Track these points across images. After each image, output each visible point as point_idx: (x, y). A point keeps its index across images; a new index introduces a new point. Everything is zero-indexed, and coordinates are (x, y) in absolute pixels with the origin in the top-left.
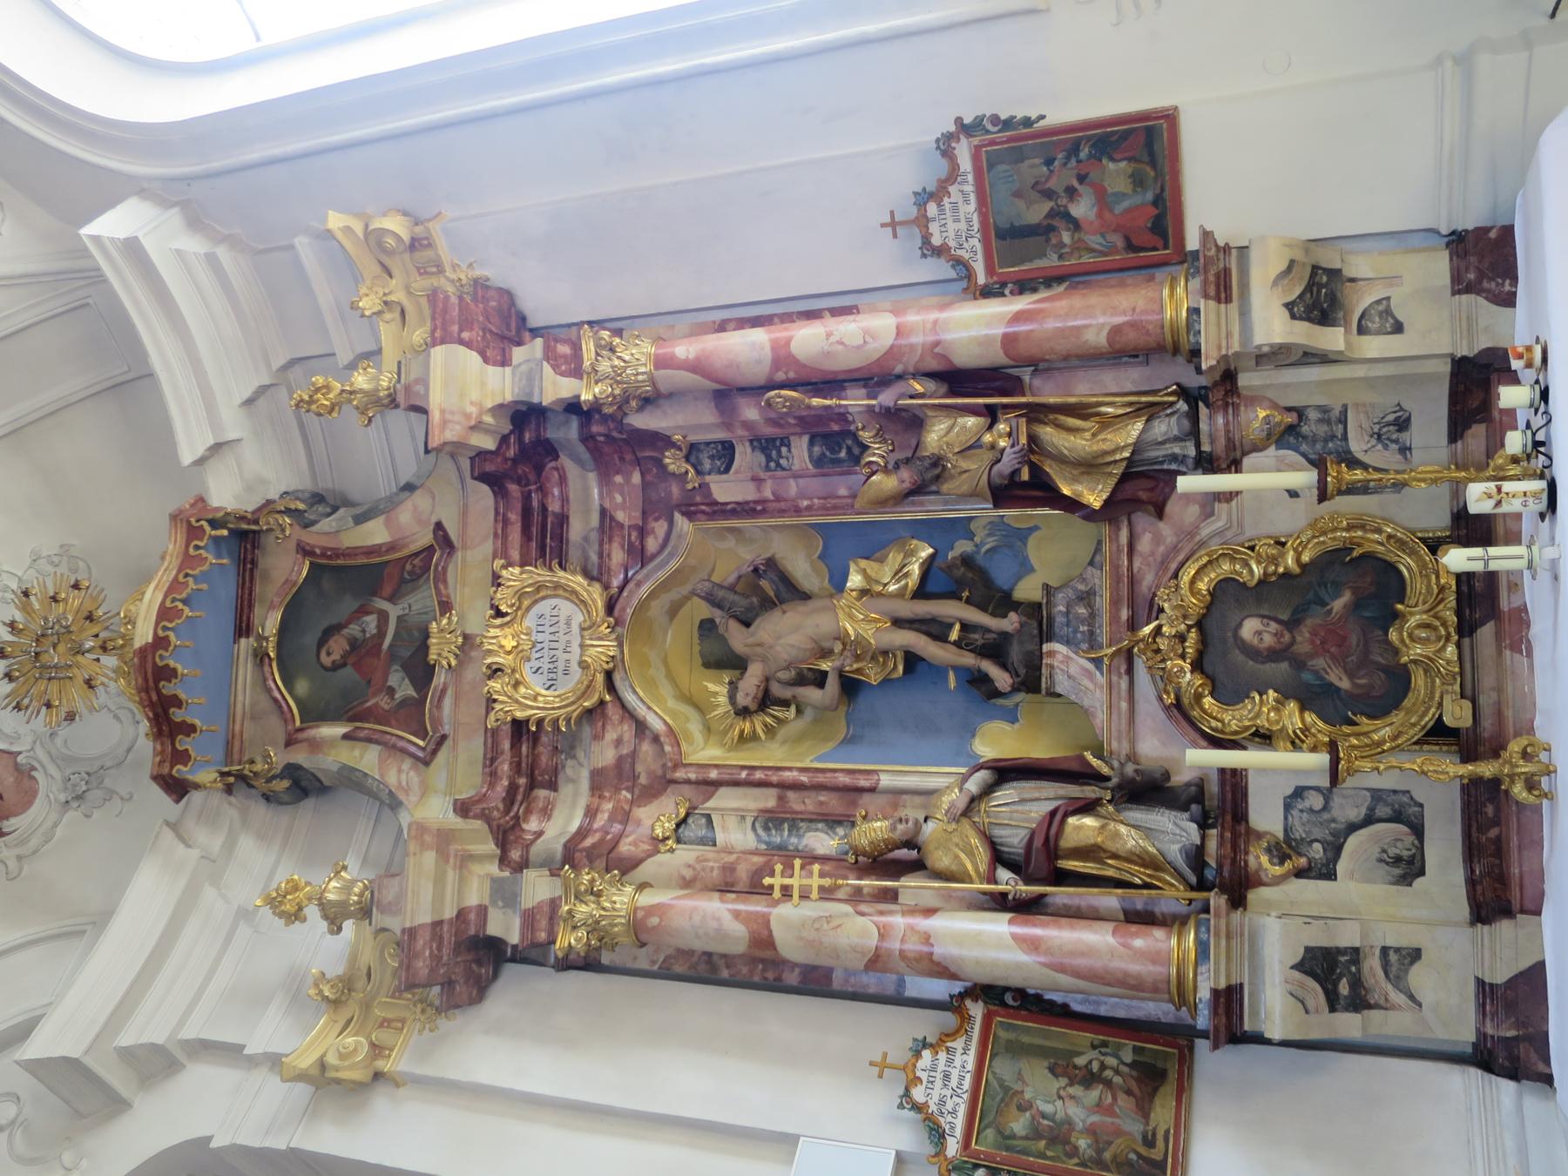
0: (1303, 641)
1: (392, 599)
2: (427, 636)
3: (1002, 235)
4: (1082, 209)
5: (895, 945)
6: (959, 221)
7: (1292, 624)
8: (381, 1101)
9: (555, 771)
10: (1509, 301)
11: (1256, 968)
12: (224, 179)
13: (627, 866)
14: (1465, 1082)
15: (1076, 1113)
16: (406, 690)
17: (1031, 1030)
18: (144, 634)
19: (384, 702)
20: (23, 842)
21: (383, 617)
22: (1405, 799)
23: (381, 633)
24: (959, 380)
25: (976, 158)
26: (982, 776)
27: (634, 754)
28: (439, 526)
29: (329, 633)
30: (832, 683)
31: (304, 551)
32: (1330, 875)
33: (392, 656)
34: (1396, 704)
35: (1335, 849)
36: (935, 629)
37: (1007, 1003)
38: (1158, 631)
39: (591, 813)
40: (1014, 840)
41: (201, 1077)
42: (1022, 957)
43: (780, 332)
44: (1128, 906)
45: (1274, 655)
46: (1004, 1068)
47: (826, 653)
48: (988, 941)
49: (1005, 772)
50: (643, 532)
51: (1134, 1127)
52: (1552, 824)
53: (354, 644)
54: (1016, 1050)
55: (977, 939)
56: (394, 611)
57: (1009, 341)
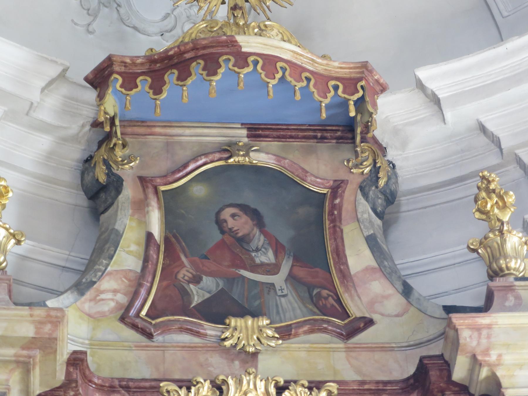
1: (291, 277)
2: (255, 315)
16: (198, 295)
18: (249, 43)
19: (185, 273)
23: (255, 268)
28: (369, 322)
29: (256, 216)
31: (337, 188)
33: (233, 280)
53: (243, 241)
56: (278, 280)
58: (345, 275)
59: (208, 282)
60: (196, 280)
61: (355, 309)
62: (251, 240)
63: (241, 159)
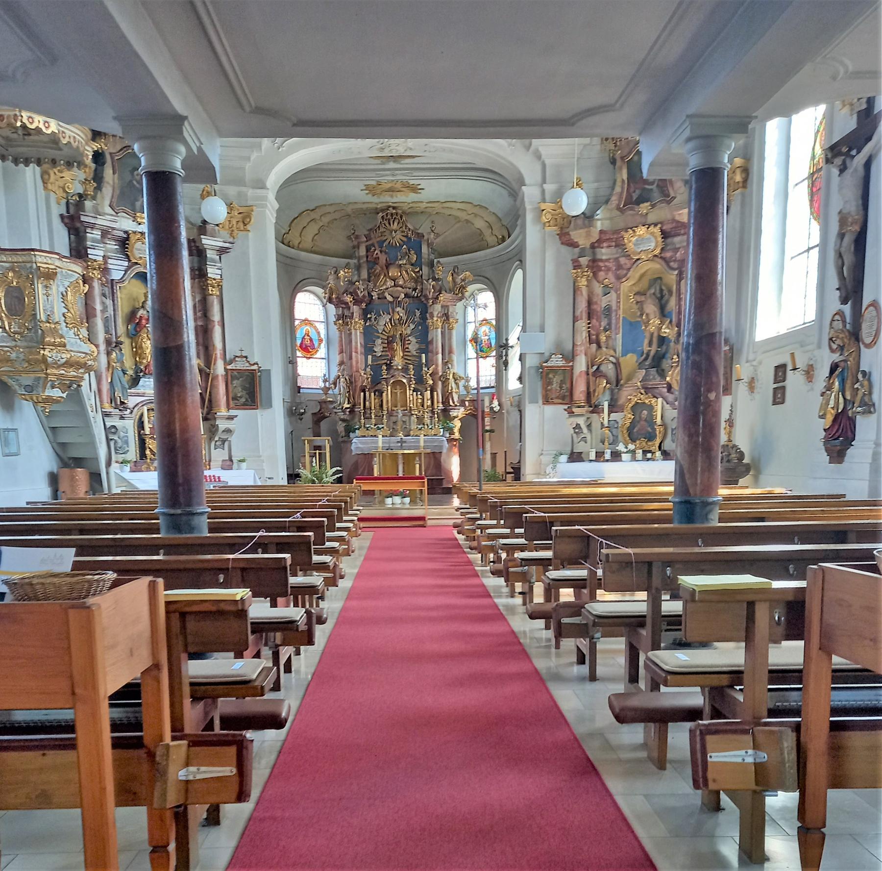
0: (643, 423)
7: (646, 420)
8: (538, 227)
13: (595, 275)
15: (554, 385)
16: (635, 196)
19: (632, 190)
26: (614, 360)
27: (623, 269)
28: (674, 198)
39: (607, 260)
43: (793, 179)
44: (781, 630)
45: (640, 417)
47: (647, 315)
48: (581, 365)
49: (617, 365)
50: (675, 261)
52: (233, 676)
61: (672, 194)
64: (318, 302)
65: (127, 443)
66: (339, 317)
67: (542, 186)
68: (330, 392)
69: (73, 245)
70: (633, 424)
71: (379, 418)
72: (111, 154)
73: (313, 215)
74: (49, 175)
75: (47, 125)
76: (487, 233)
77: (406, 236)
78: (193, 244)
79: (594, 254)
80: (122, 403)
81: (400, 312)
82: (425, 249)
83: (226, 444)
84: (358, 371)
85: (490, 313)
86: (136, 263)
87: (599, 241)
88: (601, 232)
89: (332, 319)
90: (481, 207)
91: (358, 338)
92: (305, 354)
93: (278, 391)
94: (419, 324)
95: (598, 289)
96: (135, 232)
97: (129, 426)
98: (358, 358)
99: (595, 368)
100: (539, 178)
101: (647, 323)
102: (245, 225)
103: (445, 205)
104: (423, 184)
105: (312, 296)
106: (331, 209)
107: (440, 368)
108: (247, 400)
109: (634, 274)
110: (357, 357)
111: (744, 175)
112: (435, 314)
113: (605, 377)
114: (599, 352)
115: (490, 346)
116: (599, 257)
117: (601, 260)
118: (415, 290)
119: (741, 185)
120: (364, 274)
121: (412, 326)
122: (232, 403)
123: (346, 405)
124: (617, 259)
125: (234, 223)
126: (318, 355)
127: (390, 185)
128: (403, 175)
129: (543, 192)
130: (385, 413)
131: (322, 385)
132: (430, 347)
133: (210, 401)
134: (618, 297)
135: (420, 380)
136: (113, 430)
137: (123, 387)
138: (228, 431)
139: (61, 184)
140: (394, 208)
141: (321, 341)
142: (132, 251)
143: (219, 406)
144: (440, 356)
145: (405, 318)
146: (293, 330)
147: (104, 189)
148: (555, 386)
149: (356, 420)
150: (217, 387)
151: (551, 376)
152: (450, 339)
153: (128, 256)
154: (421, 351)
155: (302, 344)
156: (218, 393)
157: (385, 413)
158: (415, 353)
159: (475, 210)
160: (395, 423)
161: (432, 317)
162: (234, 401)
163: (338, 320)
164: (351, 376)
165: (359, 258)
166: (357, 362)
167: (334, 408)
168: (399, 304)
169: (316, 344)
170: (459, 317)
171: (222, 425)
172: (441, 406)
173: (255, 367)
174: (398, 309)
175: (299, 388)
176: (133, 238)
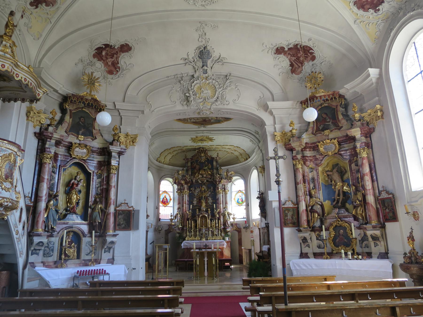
1: (332, 123)
2: (328, 129)
3: (384, 200)
4: (387, 210)
5: (301, 198)
6: (384, 195)
8: (274, 142)
9: (315, 150)
10: (378, 258)
11: (304, 233)
12: (383, 84)
13: (305, 163)
14: (299, 251)
15: (289, 217)
16: (321, 128)
17: (295, 212)
18: (317, 95)
19: (319, 125)
20: (292, 77)
21: (329, 122)
22: (99, 188)
23: (327, 122)
24: (364, 196)
25: (390, 197)
26: (320, 203)
28: (342, 127)
29: (326, 114)
30: (331, 183)
31: (337, 106)
32: (317, 240)
33: (325, 125)
34: (335, 246)
35: (320, 240)
36: (339, 195)
37: (297, 209)
38: (339, 221)
39: (310, 157)
40: (315, 208)
41: (271, 118)
42: (302, 210)
45: (339, 234)
46: (291, 210)
47: (335, 181)
48: (303, 206)
49: (322, 206)
51: (289, 223)
53: (325, 118)
54: (293, 210)
55: (303, 206)
56: (330, 123)
57: (369, 203)
58: (339, 121)
59: (322, 126)
60: (320, 126)
61: (340, 125)
62: (185, 151)
63: (98, 288)
64: (171, 184)
65: (53, 250)
66: (178, 190)
67: (274, 126)
68: (173, 221)
69: (39, 147)
70: (335, 237)
71: (195, 232)
72: (70, 110)
73: (170, 151)
74: (30, 113)
75: (17, 76)
76: (240, 157)
77: (207, 159)
78: (105, 150)
79: (303, 154)
80: (52, 228)
81: (204, 188)
82: (215, 163)
83: (111, 250)
84: (186, 212)
85: (243, 188)
86: (75, 158)
87: (305, 148)
88: (306, 143)
89: (176, 190)
90: (237, 147)
91: (186, 198)
92: (163, 205)
93: (143, 222)
94: (213, 192)
95: (307, 170)
96: (75, 143)
97: (55, 240)
98: (186, 206)
99: (310, 207)
100: (272, 122)
101: (335, 186)
102: (133, 142)
103: (223, 147)
104: (215, 137)
105: (168, 182)
106: (177, 149)
107: (222, 210)
108: (125, 226)
109: (325, 162)
110: (185, 206)
111: (382, 113)
112: (220, 188)
113: (317, 212)
114: (311, 200)
115: (242, 201)
116: (305, 155)
117: (307, 157)
118: (211, 179)
119: (380, 117)
120: (190, 173)
121: (210, 193)
122: (117, 228)
123: (181, 227)
124: (315, 156)
125: (128, 141)
126: (169, 205)
127: (201, 138)
128: (207, 133)
129: (275, 128)
130: (198, 230)
131: (170, 218)
132: (217, 201)
133: (105, 226)
134: (318, 173)
135: (213, 216)
136: (41, 244)
137: (54, 220)
138: (112, 243)
139: (39, 119)
140: (202, 148)
141: (171, 199)
142: (73, 152)
143: (109, 229)
144: (222, 205)
145: (206, 190)
146: (159, 195)
147: (63, 124)
148: (289, 217)
149: (185, 233)
150: (109, 219)
151: (286, 212)
152: (226, 198)
153: (71, 155)
154: (213, 203)
155: (162, 201)
156: (109, 222)
157: (198, 230)
158: (211, 204)
159: (235, 149)
160: (202, 234)
161: (218, 189)
162: (118, 226)
163: (178, 190)
164: (183, 214)
165: (188, 167)
166: (186, 208)
167: (175, 227)
168: (204, 184)
169: (169, 200)
170: (229, 189)
171: (109, 239)
172: (222, 227)
173: (131, 209)
174: (204, 186)
175: (160, 219)
176: (74, 147)
